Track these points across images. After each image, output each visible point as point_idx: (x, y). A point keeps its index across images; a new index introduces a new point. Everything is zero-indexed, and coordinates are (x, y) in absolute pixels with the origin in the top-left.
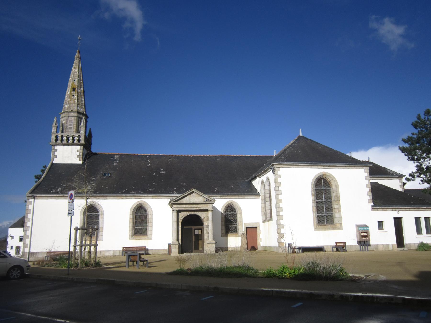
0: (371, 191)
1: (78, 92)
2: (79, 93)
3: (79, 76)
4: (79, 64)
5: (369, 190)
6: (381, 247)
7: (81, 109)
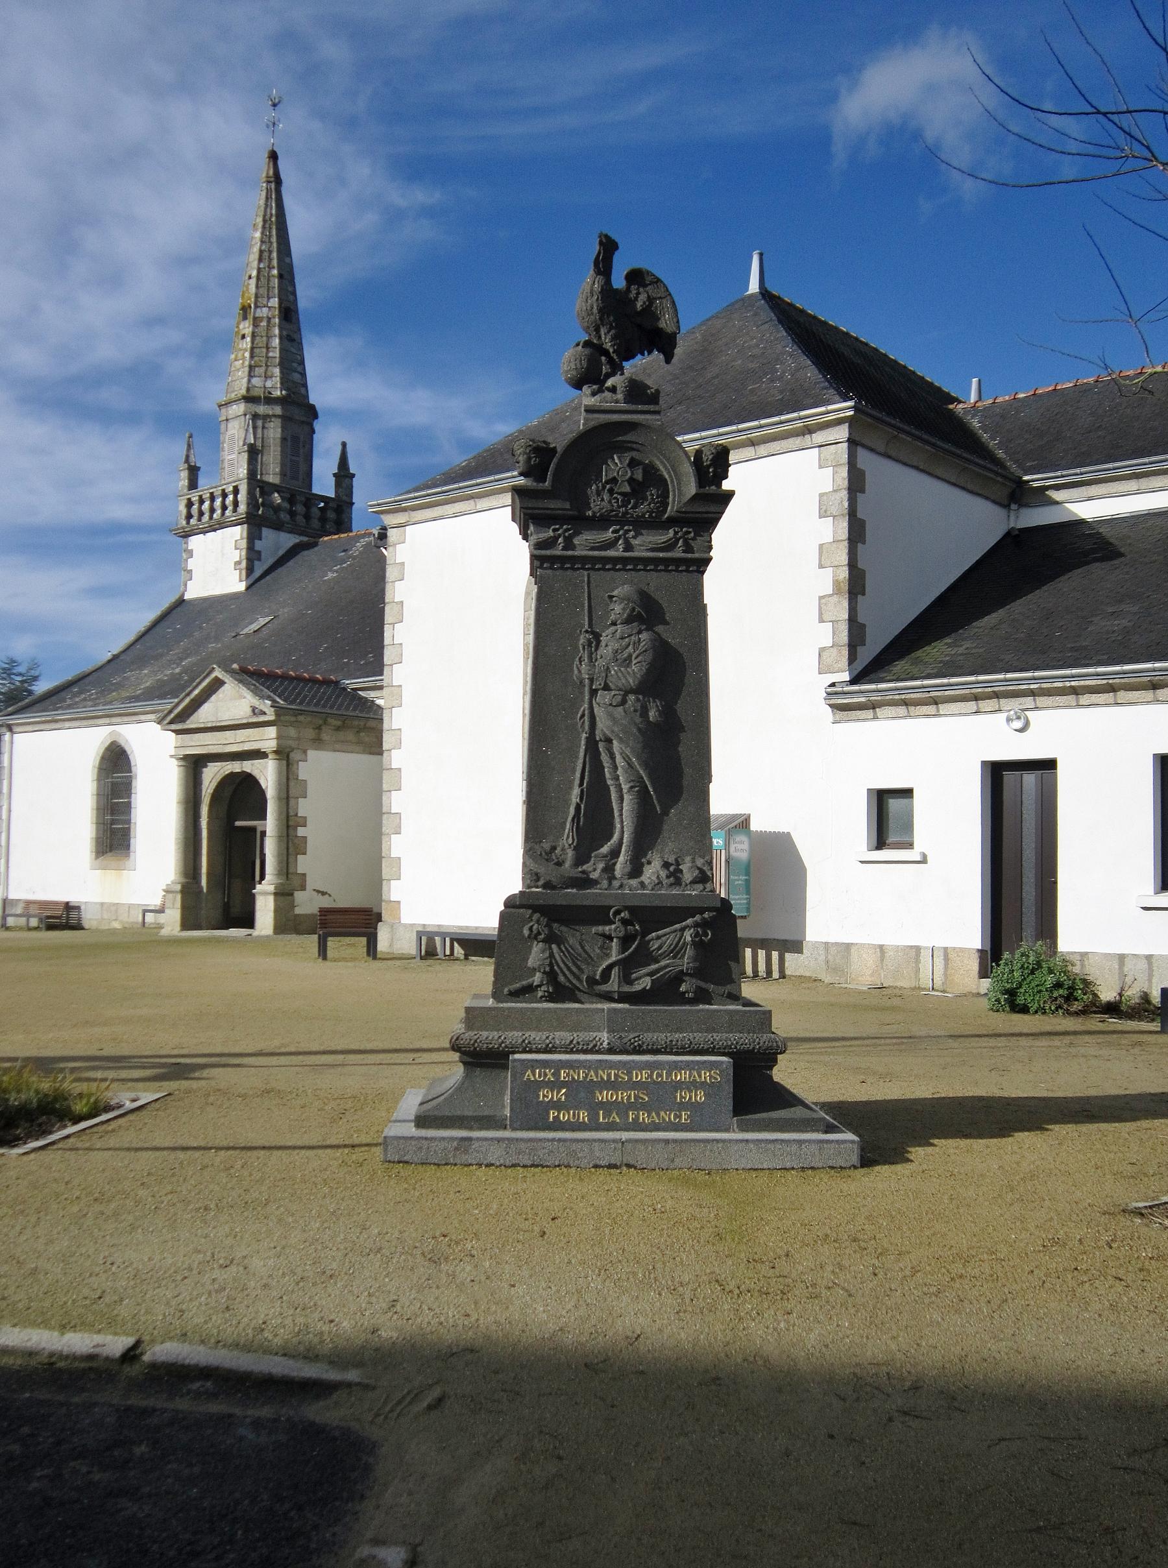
0: (845, 587)
1: (255, 319)
2: (261, 321)
3: (266, 254)
4: (266, 205)
5: (836, 583)
6: (870, 960)
7: (265, 381)
